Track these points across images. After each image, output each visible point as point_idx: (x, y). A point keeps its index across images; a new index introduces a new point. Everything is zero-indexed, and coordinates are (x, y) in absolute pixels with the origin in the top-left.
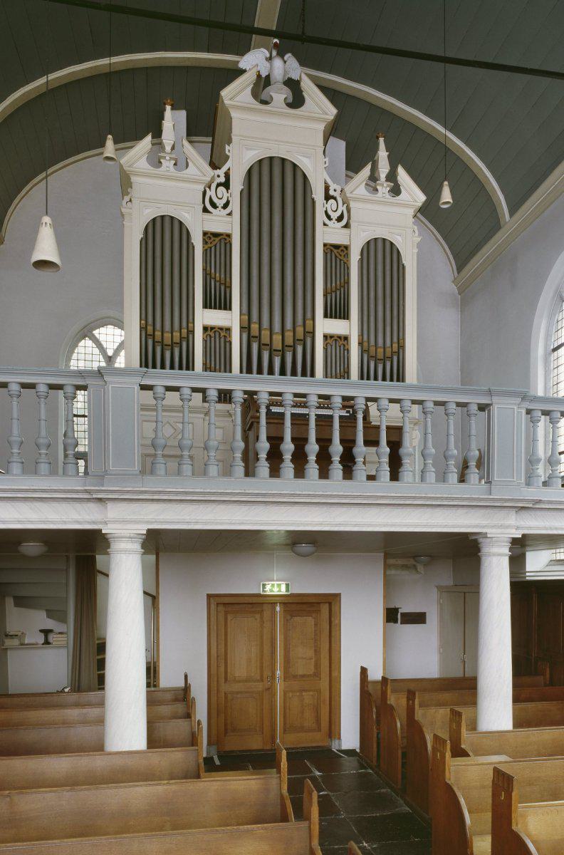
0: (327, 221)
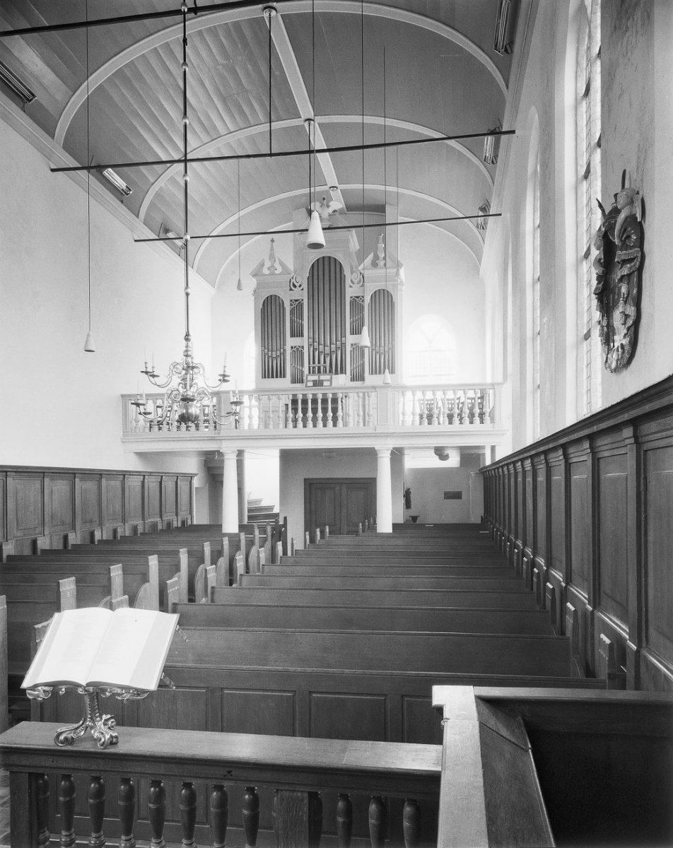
0: (351, 284)
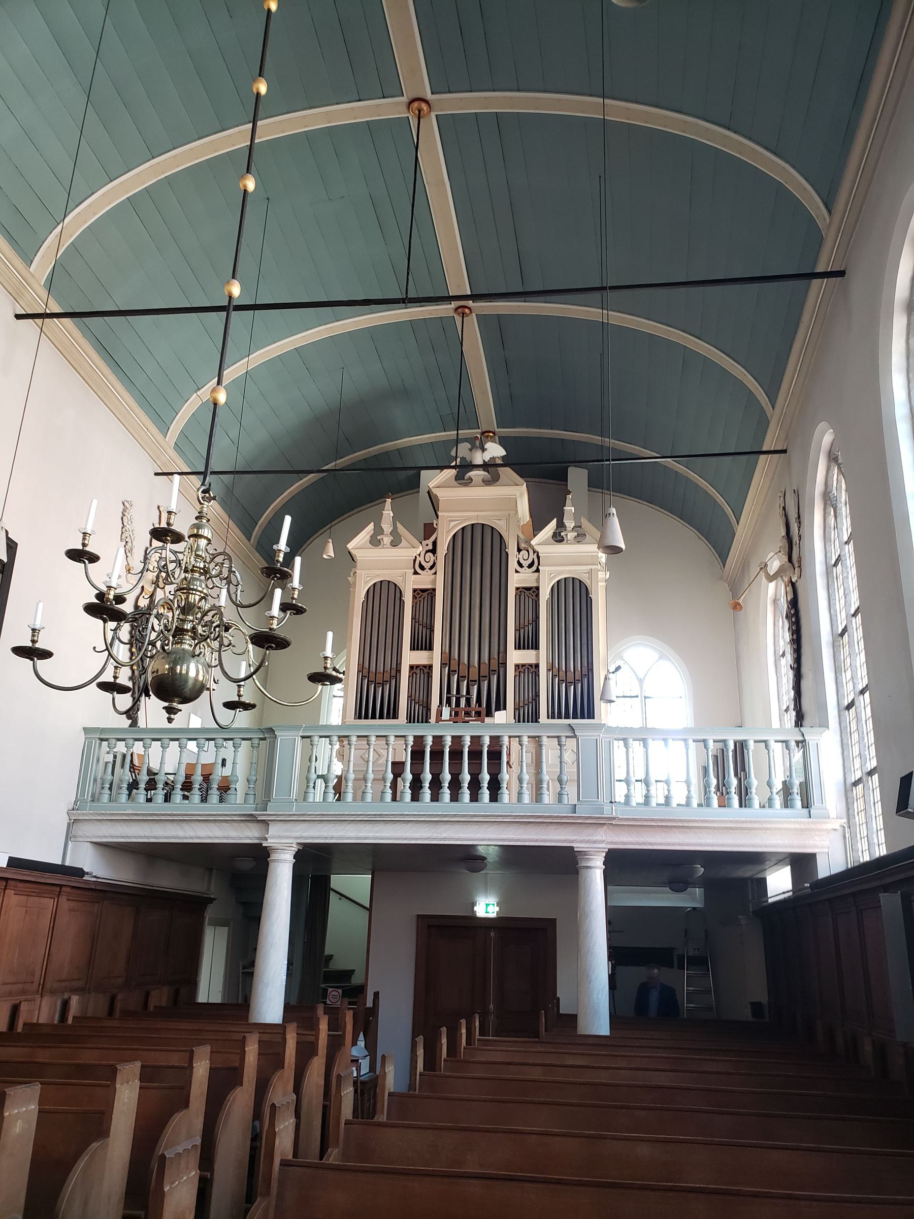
0: (519, 569)
